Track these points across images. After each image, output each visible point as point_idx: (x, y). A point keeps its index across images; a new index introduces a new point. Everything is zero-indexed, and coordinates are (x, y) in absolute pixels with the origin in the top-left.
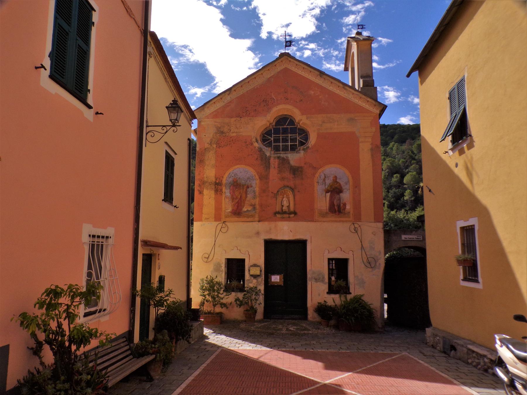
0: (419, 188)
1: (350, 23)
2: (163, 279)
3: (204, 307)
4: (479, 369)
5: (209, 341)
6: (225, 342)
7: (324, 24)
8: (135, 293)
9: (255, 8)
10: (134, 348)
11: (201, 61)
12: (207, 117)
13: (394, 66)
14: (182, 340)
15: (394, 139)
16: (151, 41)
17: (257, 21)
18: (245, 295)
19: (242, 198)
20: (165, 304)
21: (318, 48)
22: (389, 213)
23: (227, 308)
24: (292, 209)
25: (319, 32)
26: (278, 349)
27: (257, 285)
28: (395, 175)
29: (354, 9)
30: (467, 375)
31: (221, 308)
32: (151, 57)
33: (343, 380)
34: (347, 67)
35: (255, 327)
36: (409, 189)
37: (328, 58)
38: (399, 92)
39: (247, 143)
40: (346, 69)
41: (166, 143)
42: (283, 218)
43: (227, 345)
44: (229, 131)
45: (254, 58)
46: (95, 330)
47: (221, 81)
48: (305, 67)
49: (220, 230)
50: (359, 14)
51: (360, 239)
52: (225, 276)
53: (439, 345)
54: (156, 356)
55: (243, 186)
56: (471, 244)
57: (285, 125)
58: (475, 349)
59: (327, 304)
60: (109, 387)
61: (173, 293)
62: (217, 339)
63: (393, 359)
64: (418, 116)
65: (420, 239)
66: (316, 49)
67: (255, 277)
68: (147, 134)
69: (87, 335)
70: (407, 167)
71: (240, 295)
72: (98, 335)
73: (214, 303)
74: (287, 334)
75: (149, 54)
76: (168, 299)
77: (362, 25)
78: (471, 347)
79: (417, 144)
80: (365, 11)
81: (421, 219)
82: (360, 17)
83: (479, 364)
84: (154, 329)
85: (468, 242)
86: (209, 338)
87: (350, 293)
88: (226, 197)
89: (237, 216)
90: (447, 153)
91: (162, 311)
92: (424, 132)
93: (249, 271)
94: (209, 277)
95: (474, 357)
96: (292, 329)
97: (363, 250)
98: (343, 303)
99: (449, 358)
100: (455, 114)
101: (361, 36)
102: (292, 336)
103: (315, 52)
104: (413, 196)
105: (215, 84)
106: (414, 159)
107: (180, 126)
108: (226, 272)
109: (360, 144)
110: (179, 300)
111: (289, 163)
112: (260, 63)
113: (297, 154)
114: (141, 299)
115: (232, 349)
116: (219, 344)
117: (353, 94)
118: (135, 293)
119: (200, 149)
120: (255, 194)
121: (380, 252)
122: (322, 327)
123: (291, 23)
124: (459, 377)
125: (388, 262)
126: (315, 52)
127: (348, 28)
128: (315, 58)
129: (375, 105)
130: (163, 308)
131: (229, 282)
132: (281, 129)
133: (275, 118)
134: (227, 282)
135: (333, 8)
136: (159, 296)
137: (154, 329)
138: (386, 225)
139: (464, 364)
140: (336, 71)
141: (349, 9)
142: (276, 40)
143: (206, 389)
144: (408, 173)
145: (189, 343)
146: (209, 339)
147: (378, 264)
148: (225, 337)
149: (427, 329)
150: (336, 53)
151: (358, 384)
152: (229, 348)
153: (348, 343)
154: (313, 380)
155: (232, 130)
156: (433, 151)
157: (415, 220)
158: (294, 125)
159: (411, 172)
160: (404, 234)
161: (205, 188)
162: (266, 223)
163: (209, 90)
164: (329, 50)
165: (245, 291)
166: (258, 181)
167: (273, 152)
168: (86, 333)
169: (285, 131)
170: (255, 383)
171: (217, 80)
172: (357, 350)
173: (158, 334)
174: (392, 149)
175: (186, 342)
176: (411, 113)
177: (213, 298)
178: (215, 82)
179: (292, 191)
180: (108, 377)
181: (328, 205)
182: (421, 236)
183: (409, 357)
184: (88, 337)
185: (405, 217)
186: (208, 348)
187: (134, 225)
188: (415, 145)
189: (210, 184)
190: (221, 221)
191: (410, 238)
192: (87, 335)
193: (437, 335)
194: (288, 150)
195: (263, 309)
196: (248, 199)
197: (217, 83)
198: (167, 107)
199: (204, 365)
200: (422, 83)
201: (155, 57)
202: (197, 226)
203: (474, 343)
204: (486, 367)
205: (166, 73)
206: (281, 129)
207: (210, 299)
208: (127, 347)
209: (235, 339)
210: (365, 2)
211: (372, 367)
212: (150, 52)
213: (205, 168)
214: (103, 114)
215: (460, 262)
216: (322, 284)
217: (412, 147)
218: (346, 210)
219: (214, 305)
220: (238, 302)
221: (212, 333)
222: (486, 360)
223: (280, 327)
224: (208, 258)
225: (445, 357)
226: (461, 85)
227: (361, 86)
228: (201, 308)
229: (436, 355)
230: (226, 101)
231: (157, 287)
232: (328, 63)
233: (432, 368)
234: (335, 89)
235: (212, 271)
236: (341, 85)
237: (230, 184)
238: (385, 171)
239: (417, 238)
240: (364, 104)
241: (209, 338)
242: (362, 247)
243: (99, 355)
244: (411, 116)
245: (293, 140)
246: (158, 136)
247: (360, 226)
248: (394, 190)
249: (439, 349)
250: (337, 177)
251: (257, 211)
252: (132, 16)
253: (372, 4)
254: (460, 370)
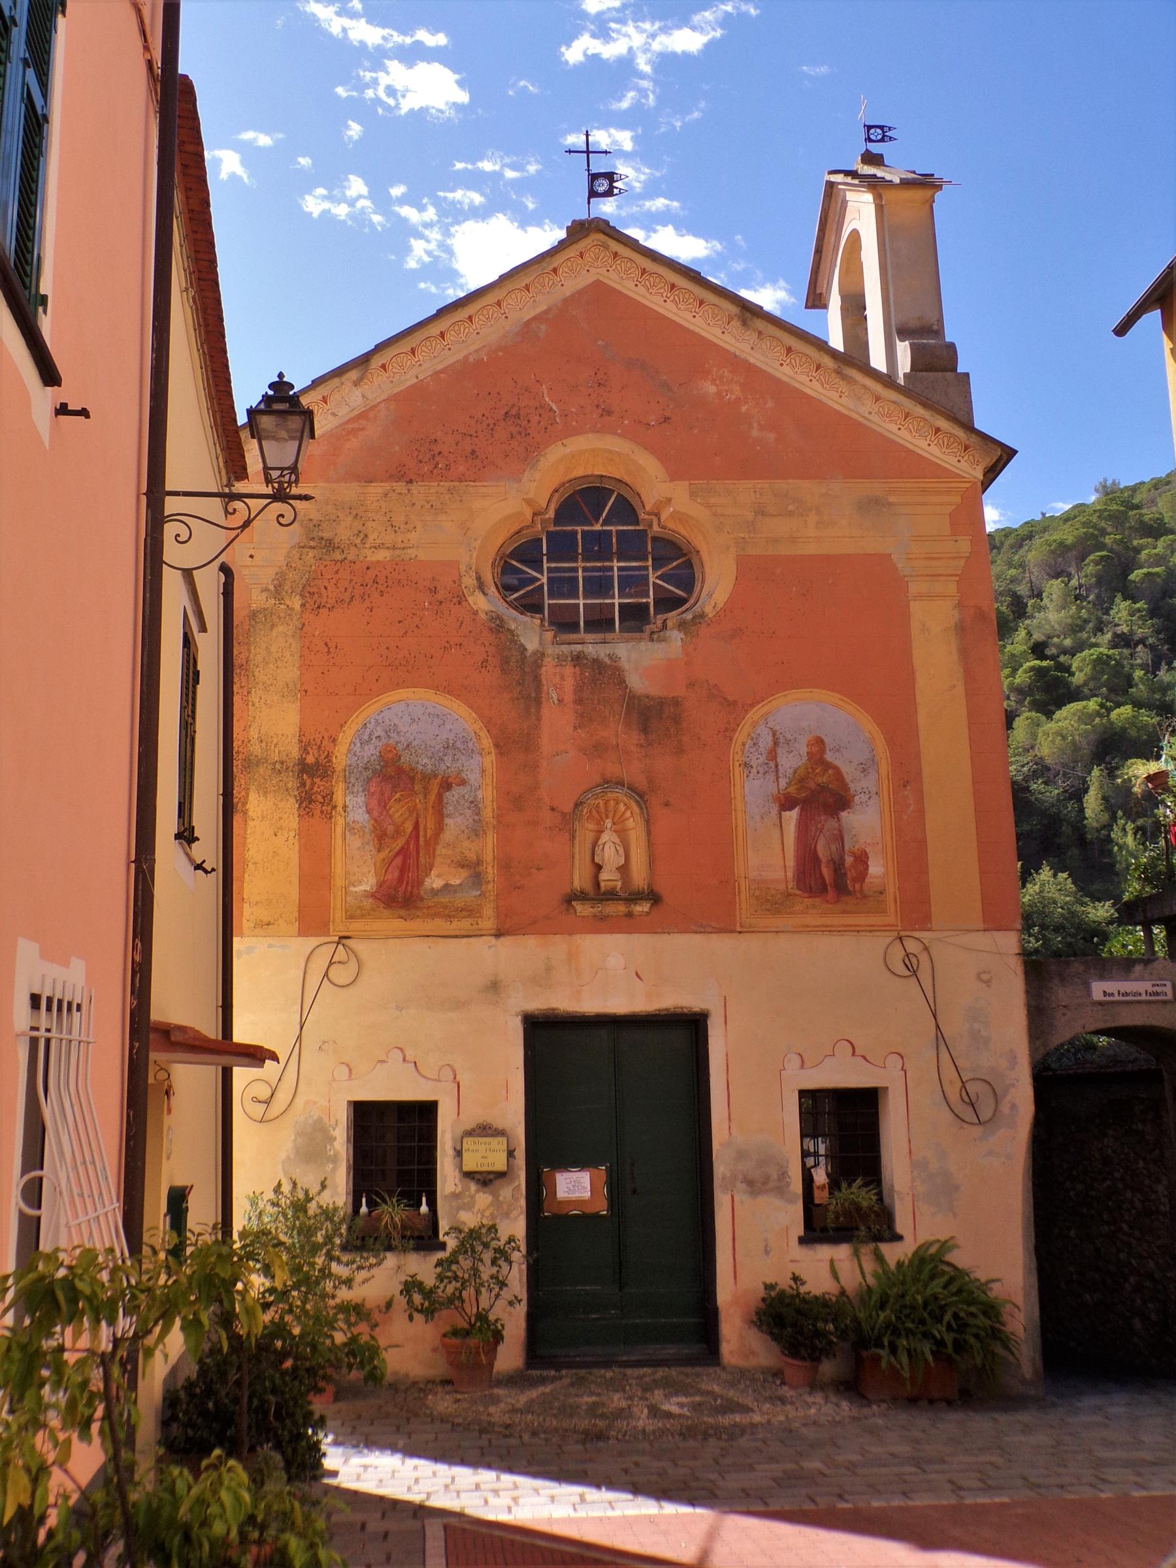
19: (421, 833)
120: (478, 814)
133: (556, 491)
237: (366, 769)
250: (826, 740)
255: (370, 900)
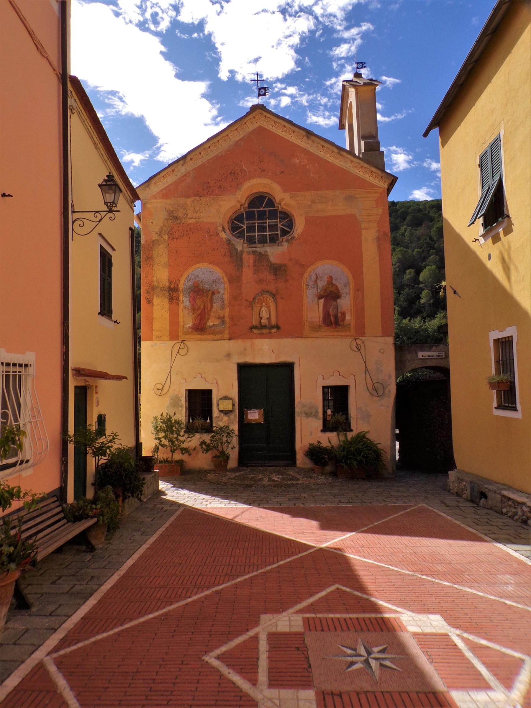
0: (440, 288)
1: (343, 55)
2: (103, 419)
3: (159, 454)
4: (516, 521)
5: (167, 498)
6: (188, 499)
7: (307, 58)
8: (66, 438)
9: (210, 35)
10: (68, 510)
11: (137, 113)
12: (154, 197)
13: (404, 118)
14: (131, 498)
15: (405, 222)
16: (72, 90)
17: (213, 55)
18: (213, 436)
20: (109, 453)
21: (299, 94)
22: (400, 323)
23: (190, 455)
24: (273, 321)
25: (299, 69)
26: (259, 506)
27: (228, 423)
28: (408, 271)
29: (346, 35)
30: (501, 529)
31: (181, 455)
32: (73, 114)
33: (344, 542)
34: (343, 123)
35: (227, 477)
36: (427, 289)
37: (314, 107)
38: (411, 155)
39: (211, 233)
40: (341, 126)
41: (100, 235)
42: (262, 334)
43: (190, 503)
44: (185, 217)
45: (211, 110)
46: (17, 488)
47: (167, 143)
48: (287, 125)
49: (178, 352)
50: (353, 43)
51: (364, 359)
52: (186, 413)
53: (465, 492)
54: (98, 520)
55: (207, 291)
56: (508, 361)
57: (262, 206)
58: (512, 496)
59: (321, 445)
60: (38, 561)
61: (118, 437)
62: (177, 495)
63: (407, 513)
64: (438, 188)
65: (442, 356)
66: (298, 95)
67: (226, 413)
68: (73, 223)
69: (6, 495)
70: (424, 259)
71: (207, 438)
72: (22, 495)
73: (172, 449)
74: (269, 485)
75: (71, 109)
76: (112, 446)
77: (362, 63)
78: (505, 493)
79: (437, 228)
80: (362, 38)
81: (443, 330)
82: (356, 47)
83: (516, 514)
84: (93, 484)
85: (505, 359)
86: (167, 494)
87: (352, 430)
88: (184, 307)
89: (200, 333)
90: (477, 241)
91: (103, 460)
92: (447, 213)
93: (218, 405)
94: (165, 414)
95: (510, 506)
96: (276, 479)
97: (367, 373)
98: (341, 443)
99: (478, 508)
100: (487, 188)
101: (361, 79)
102: (276, 488)
103: (296, 99)
104: (433, 297)
105: (159, 148)
106: (433, 248)
107: (118, 211)
108: (187, 407)
109: (363, 232)
110: (127, 446)
111: (268, 260)
112: (220, 117)
113: (280, 247)
114: (74, 446)
115: (197, 507)
116: (180, 501)
117: (352, 162)
118: (66, 438)
119: (146, 241)
120: (223, 302)
121: (390, 377)
122: (315, 475)
123: (260, 58)
124: (490, 532)
125: (400, 387)
126: (296, 99)
127: (339, 62)
128: (294, 108)
129: (382, 177)
130: (105, 458)
131: (191, 421)
132: (256, 212)
133: (248, 197)
134: (189, 420)
135: (318, 34)
136: (99, 441)
137: (93, 484)
138: (397, 337)
139: (496, 514)
140: (325, 126)
141: (339, 36)
142: (241, 83)
143: (165, 561)
144: (425, 267)
145: (141, 501)
146: (166, 495)
147: (387, 391)
148: (188, 491)
149: (450, 472)
150: (324, 100)
151: (363, 546)
152: (193, 507)
153: (350, 495)
154: (305, 544)
155: (189, 215)
156: (458, 238)
157: (434, 330)
158: (274, 207)
159: (429, 266)
160: (422, 351)
161: (155, 296)
162: (240, 341)
163: (151, 157)
164: (315, 96)
165: (213, 432)
166: (227, 286)
167: (246, 245)
168: (5, 493)
169: (262, 215)
170: (230, 550)
171: (161, 142)
172: (361, 502)
173: (100, 490)
174: (403, 235)
175: (136, 500)
176: (428, 183)
177: (171, 441)
178: (158, 145)
179: (273, 297)
180: (37, 548)
181: (321, 316)
182: (444, 353)
183: (428, 509)
184: (8, 498)
185: (421, 326)
186: (166, 507)
187: (62, 347)
188: (434, 229)
189: (162, 289)
190: (178, 340)
191: (429, 356)
192: (6, 495)
193: (462, 480)
194: (266, 242)
195: (237, 454)
196: (214, 309)
197: (161, 146)
198: (100, 186)
199: (162, 529)
200: (443, 146)
201: (79, 113)
202: (145, 346)
203: (510, 488)
204: (524, 517)
205: (95, 136)
206: (256, 212)
207: (167, 443)
208: (59, 509)
209: (201, 494)
210: (362, 24)
211: (380, 524)
212: (72, 106)
213: (154, 267)
214: (12, 196)
215: (493, 385)
216: (314, 419)
217: (431, 232)
218: (345, 321)
219: (173, 451)
220: (204, 447)
221: (172, 487)
222: (525, 508)
223: (261, 476)
224: (161, 390)
225: (473, 507)
226: (495, 146)
227: (363, 150)
228: (155, 454)
229: (461, 505)
230: (179, 175)
231: (96, 430)
232: (314, 115)
233: (458, 522)
234: (328, 156)
235: (168, 406)
236: (336, 150)
238: (395, 265)
239: (437, 355)
240: (367, 176)
241: (167, 494)
242: (366, 369)
243: (23, 520)
244: (428, 189)
245: (273, 227)
246: (89, 226)
247: (363, 342)
248: (407, 290)
249: (466, 498)
250: (333, 277)
251: (227, 325)
252: (44, 54)
253: (372, 27)
254: (492, 523)
255: (191, 329)
